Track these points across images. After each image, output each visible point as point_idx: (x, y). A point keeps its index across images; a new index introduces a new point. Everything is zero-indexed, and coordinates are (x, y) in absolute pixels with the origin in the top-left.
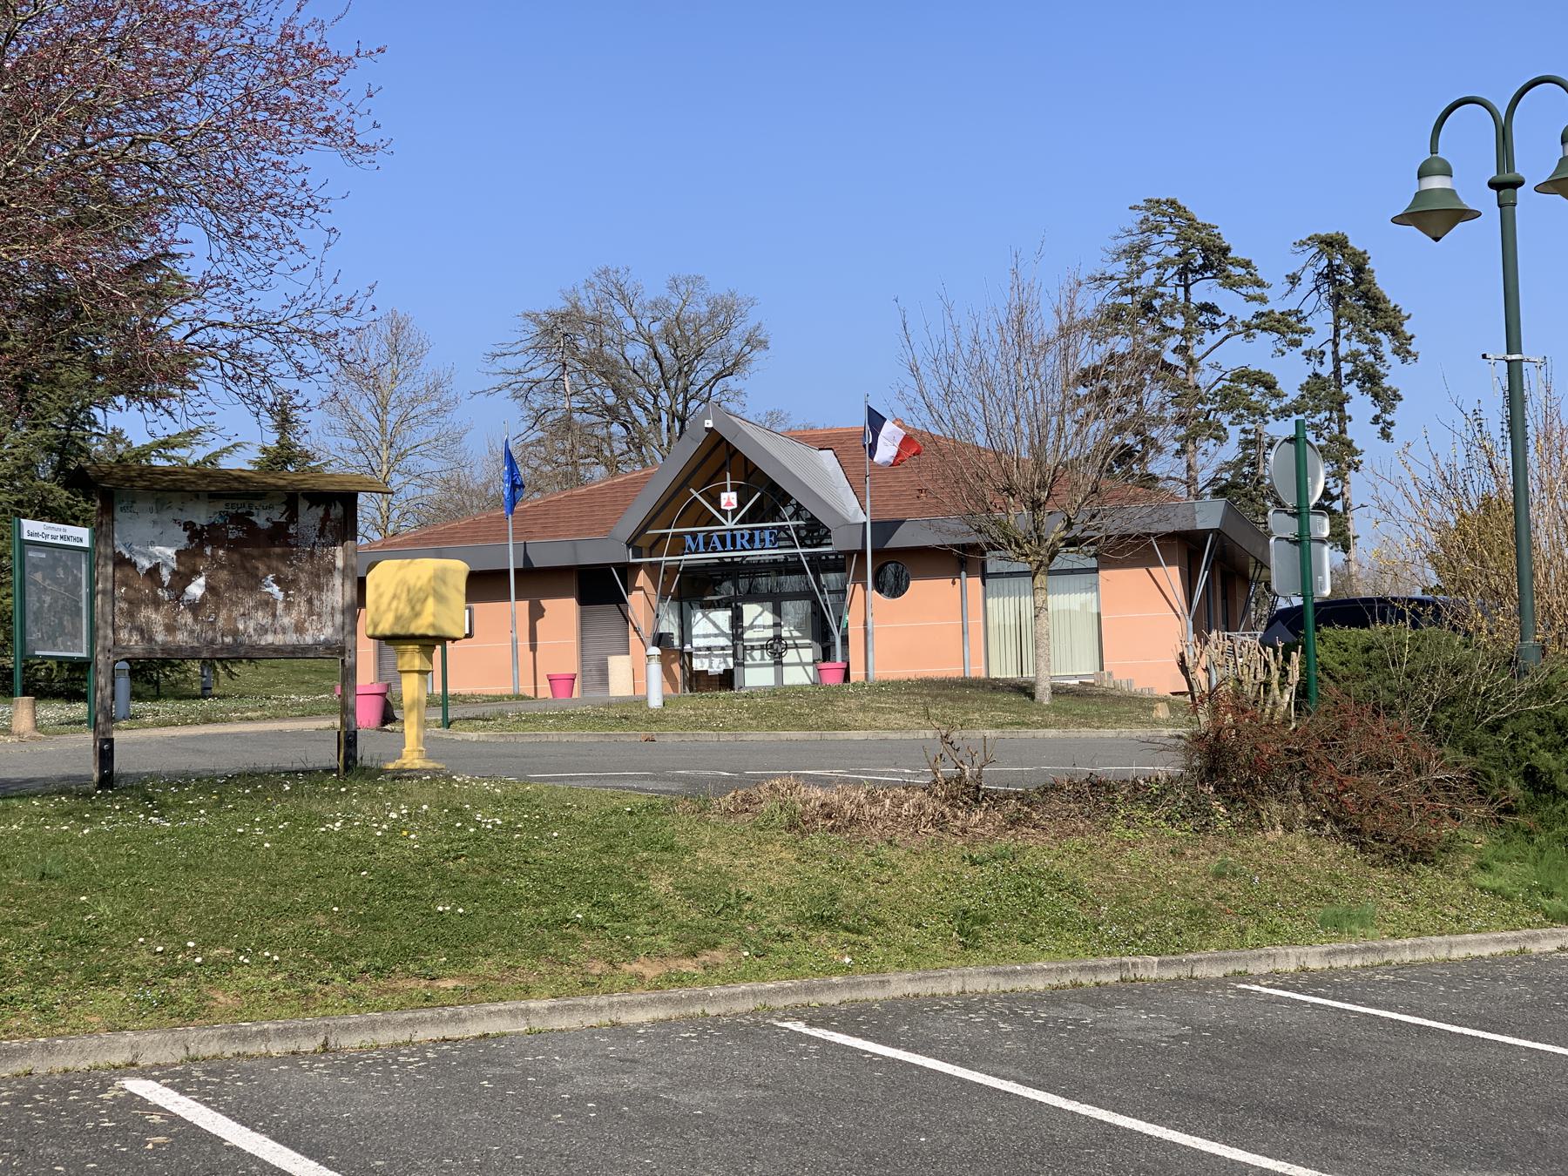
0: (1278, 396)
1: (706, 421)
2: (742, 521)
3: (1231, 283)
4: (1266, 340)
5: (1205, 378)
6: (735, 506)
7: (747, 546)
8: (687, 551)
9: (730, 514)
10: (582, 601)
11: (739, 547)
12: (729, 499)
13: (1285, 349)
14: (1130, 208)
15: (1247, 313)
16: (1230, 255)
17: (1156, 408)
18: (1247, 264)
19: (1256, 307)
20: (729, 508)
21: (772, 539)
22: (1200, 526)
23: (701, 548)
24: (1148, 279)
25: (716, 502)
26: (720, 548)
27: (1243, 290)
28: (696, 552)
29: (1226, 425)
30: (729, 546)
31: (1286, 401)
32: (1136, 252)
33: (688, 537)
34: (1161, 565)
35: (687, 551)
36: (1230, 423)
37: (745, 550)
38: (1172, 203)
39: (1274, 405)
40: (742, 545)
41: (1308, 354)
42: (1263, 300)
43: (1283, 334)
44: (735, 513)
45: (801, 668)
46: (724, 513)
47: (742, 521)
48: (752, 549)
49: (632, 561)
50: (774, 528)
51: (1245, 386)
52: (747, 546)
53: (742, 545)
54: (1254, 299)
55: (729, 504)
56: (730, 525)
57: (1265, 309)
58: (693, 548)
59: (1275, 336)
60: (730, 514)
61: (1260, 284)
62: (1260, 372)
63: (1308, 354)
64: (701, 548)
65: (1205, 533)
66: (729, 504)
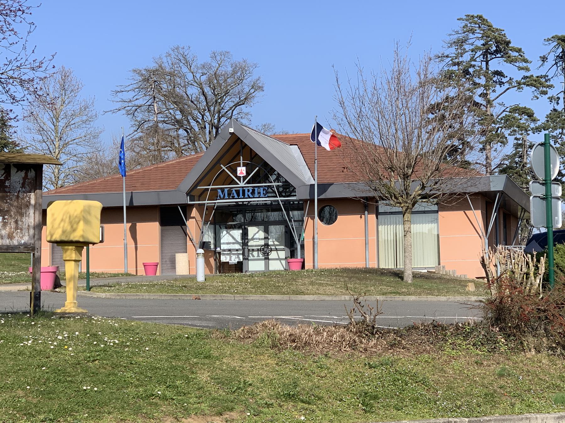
0: (534, 120)
1: (230, 129)
2: (248, 183)
3: (511, 60)
4: (528, 91)
5: (496, 111)
6: (245, 174)
7: (251, 196)
8: (218, 198)
9: (242, 179)
10: (162, 224)
11: (246, 196)
12: (242, 171)
13: (538, 96)
14: (458, 19)
15: (518, 76)
16: (510, 45)
17: (243, 170)
18: (519, 50)
19: (524, 73)
20: (241, 175)
21: (265, 192)
22: (492, 189)
23: (226, 197)
24: (466, 57)
25: (234, 172)
26: (236, 197)
27: (517, 64)
28: (223, 199)
29: (507, 136)
31: (539, 123)
32: (460, 43)
33: (219, 191)
34: (472, 209)
35: (218, 198)
36: (509, 135)
37: (250, 198)
38: (480, 17)
39: (532, 125)
40: (248, 195)
41: (551, 99)
42: (527, 69)
43: (538, 88)
44: (245, 178)
45: (279, 261)
46: (239, 178)
47: (248, 183)
48: (254, 198)
49: (189, 203)
50: (265, 186)
51: (517, 115)
52: (251, 196)
53: (248, 195)
54: (522, 69)
55: (241, 173)
56: (242, 184)
57: (528, 74)
58: (222, 196)
59: (534, 88)
60: (242, 179)
61: (526, 61)
62: (525, 108)
63: (551, 99)
64: (226, 197)
65: (495, 193)
66: (241, 173)
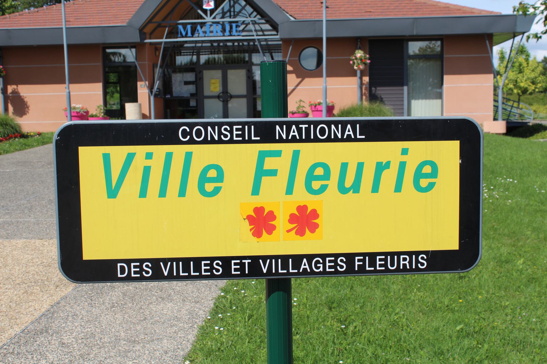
9: (209, 13)
11: (234, 33)
20: (208, 8)
28: (186, 36)
30: (227, 33)
35: (179, 36)
48: (224, 36)
58: (184, 33)
64: (189, 34)
